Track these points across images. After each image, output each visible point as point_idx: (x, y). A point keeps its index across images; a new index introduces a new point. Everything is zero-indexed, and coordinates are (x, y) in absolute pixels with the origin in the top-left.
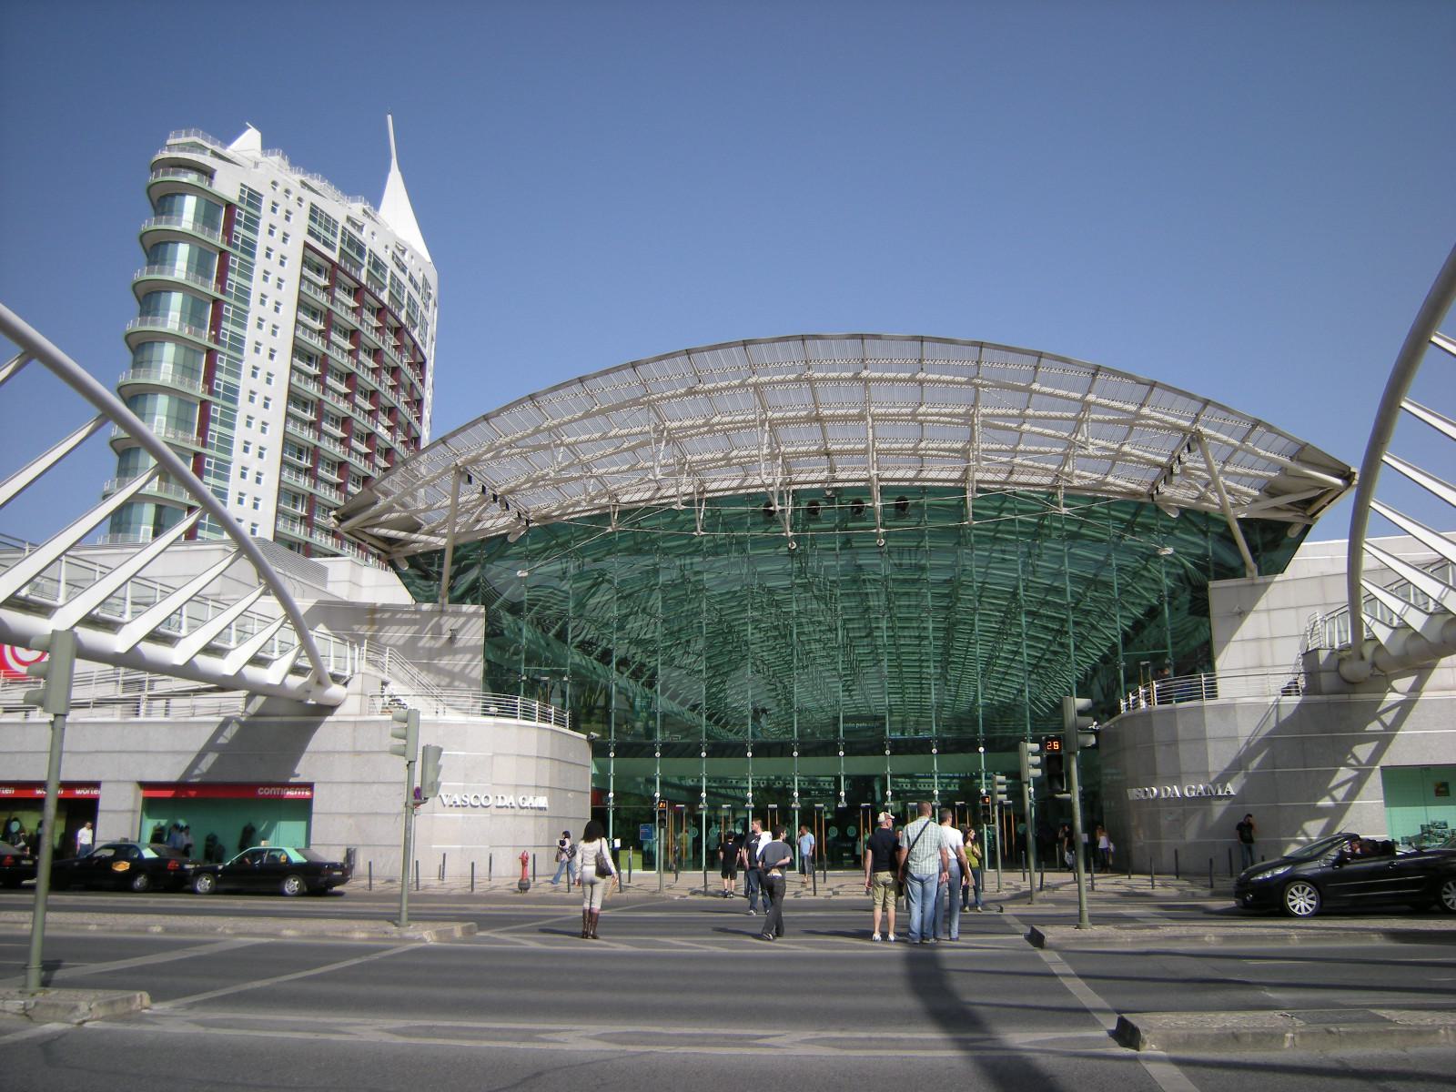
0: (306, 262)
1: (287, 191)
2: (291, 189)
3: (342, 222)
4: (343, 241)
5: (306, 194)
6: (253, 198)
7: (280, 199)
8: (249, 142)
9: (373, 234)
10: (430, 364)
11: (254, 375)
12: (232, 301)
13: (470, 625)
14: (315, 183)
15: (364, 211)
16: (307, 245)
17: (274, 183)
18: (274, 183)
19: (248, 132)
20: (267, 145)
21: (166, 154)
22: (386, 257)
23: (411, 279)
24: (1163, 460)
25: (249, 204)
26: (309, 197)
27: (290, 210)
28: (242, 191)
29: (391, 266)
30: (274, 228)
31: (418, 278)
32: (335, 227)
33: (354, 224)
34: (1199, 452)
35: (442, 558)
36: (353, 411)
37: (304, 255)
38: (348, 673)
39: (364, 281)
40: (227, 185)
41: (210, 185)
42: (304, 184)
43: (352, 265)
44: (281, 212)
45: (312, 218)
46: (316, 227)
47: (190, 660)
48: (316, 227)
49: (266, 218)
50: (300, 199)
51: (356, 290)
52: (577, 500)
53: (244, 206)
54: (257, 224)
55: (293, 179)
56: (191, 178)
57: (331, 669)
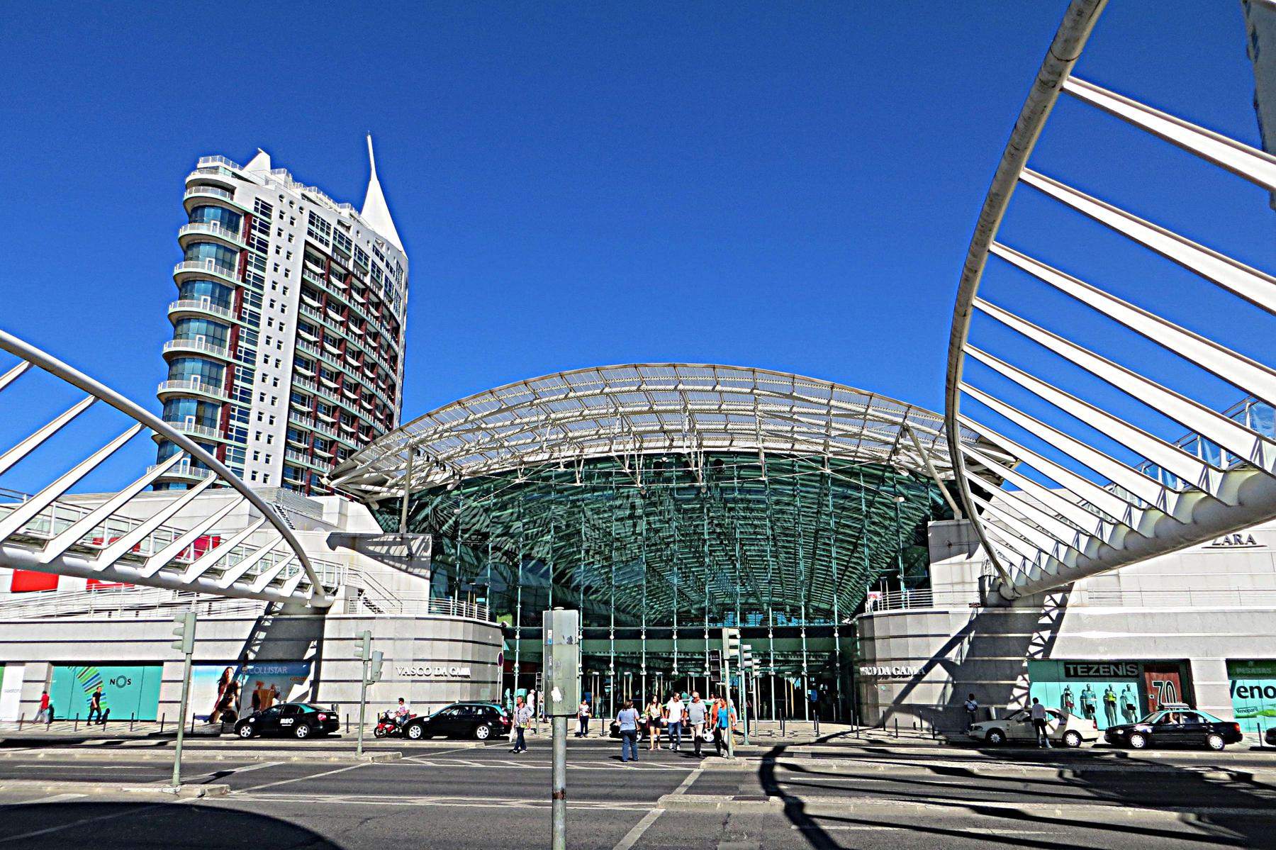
0: (307, 256)
1: (291, 203)
2: (294, 200)
3: (334, 224)
4: (335, 238)
5: (306, 204)
6: (266, 209)
7: (286, 208)
8: (263, 159)
9: (358, 232)
10: (403, 328)
11: (268, 342)
12: (250, 287)
13: (421, 544)
14: (312, 194)
15: (351, 215)
16: (307, 243)
17: (281, 197)
18: (281, 197)
19: (259, 156)
20: (274, 166)
21: (188, 180)
22: (368, 250)
23: (388, 265)
24: (893, 440)
25: (262, 213)
26: (309, 207)
27: (294, 216)
28: (257, 203)
29: (372, 256)
30: (282, 230)
31: (393, 264)
32: (329, 228)
33: (343, 225)
34: (908, 437)
35: (402, 502)
36: (347, 334)
37: (305, 251)
38: (335, 586)
39: (351, 268)
40: (244, 201)
41: (232, 199)
42: (304, 196)
43: (342, 257)
44: (287, 218)
45: (311, 223)
46: (314, 229)
47: (231, 585)
48: (314, 229)
49: (275, 223)
50: (301, 208)
51: (346, 276)
52: (498, 462)
53: (258, 215)
54: (268, 228)
55: (296, 191)
56: (211, 193)
57: (324, 584)
